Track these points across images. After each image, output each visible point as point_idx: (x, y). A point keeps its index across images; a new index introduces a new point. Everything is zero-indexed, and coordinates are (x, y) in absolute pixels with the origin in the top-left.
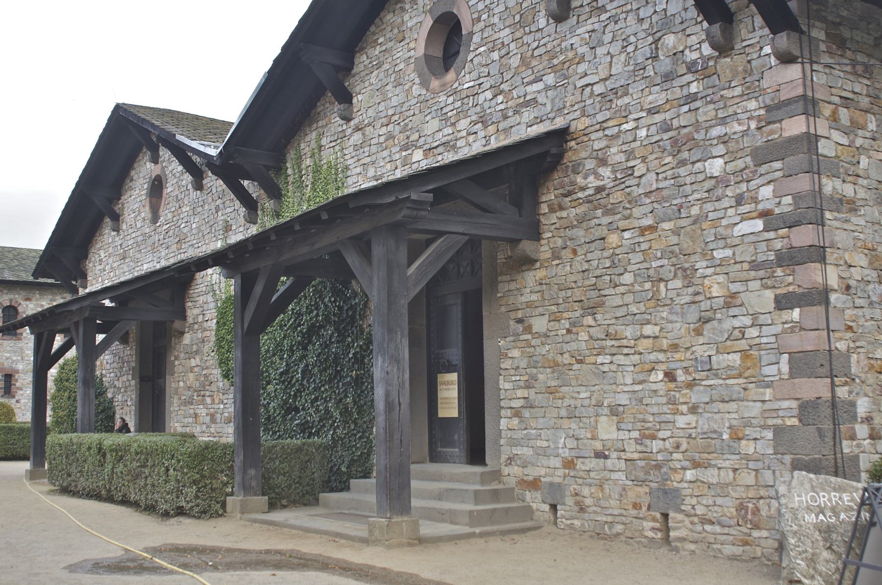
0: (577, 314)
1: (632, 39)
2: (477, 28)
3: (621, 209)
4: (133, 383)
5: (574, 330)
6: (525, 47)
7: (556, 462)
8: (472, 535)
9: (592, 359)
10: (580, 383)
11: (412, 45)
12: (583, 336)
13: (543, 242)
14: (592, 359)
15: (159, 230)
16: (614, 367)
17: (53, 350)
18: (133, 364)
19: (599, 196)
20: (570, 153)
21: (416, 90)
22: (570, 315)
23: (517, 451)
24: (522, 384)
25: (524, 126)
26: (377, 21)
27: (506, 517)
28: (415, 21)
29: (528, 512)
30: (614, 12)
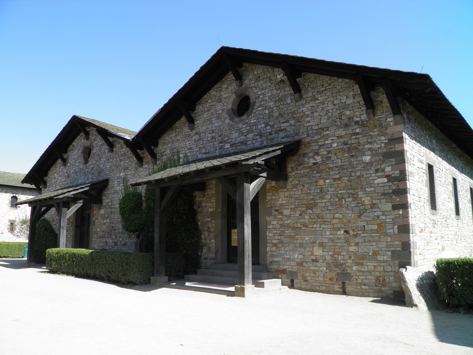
21: (227, 121)
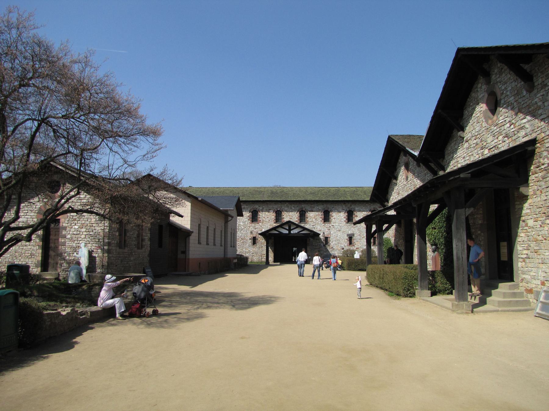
0: (544, 219)
2: (502, 97)
8: (497, 311)
13: (530, 187)
21: (484, 124)
22: (541, 219)
23: (524, 276)
24: (525, 248)
25: (521, 138)
27: (520, 306)
28: (482, 95)
29: (528, 302)
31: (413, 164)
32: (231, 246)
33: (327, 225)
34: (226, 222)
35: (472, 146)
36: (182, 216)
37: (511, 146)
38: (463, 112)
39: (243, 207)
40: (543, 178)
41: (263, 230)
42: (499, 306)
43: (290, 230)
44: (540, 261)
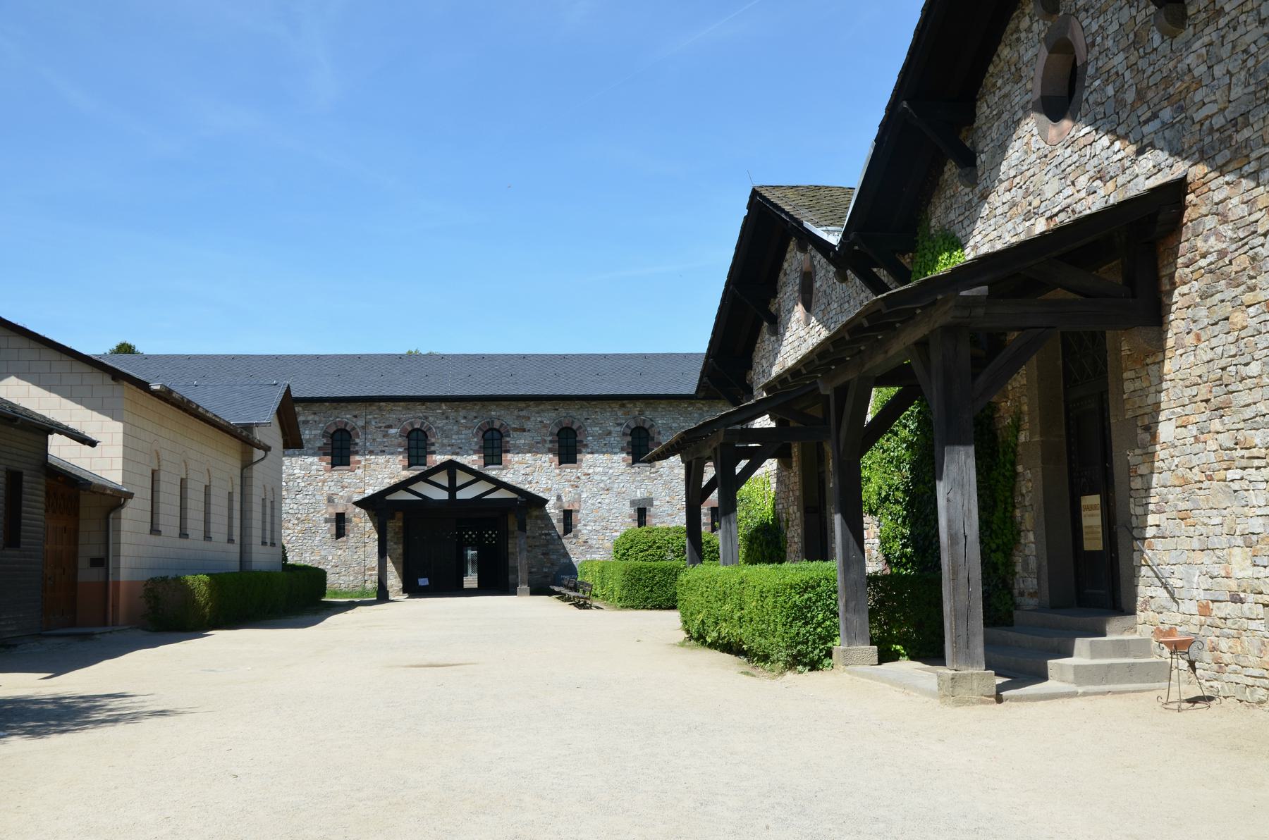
1: (1253, 49)
3: (1245, 278)
4: (798, 514)
5: (1202, 437)
6: (1140, 75)
7: (1193, 607)
9: (1222, 474)
10: (1211, 505)
11: (1029, 86)
12: (1212, 445)
14: (1222, 474)
15: (812, 332)
16: (1245, 484)
17: (704, 483)
18: (797, 493)
19: (1221, 263)
20: (1189, 210)
25: (1142, 178)
26: (995, 58)
28: (1030, 53)
30: (1234, 13)
31: (825, 273)
32: (264, 543)
33: (569, 470)
34: (247, 464)
35: (999, 211)
36: (93, 444)
37: (1112, 201)
38: (975, 107)
39: (301, 419)
40: (1204, 296)
41: (370, 492)
42: (1078, 682)
43: (452, 489)
44: (1196, 545)
